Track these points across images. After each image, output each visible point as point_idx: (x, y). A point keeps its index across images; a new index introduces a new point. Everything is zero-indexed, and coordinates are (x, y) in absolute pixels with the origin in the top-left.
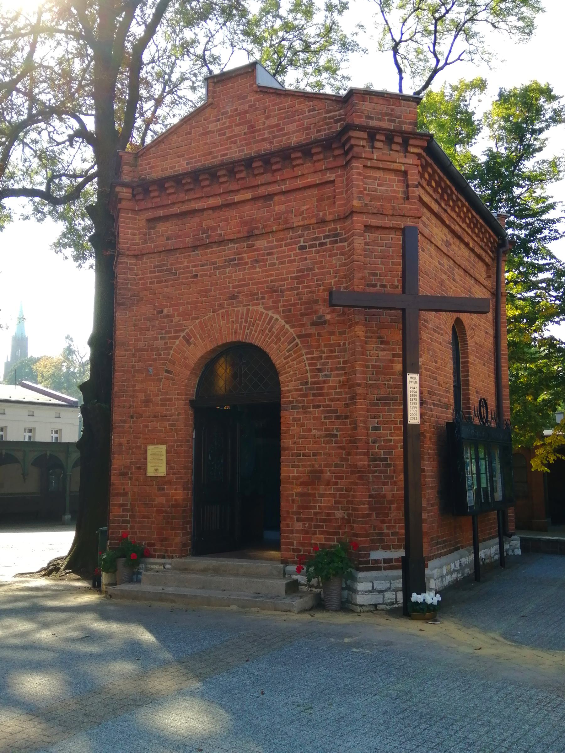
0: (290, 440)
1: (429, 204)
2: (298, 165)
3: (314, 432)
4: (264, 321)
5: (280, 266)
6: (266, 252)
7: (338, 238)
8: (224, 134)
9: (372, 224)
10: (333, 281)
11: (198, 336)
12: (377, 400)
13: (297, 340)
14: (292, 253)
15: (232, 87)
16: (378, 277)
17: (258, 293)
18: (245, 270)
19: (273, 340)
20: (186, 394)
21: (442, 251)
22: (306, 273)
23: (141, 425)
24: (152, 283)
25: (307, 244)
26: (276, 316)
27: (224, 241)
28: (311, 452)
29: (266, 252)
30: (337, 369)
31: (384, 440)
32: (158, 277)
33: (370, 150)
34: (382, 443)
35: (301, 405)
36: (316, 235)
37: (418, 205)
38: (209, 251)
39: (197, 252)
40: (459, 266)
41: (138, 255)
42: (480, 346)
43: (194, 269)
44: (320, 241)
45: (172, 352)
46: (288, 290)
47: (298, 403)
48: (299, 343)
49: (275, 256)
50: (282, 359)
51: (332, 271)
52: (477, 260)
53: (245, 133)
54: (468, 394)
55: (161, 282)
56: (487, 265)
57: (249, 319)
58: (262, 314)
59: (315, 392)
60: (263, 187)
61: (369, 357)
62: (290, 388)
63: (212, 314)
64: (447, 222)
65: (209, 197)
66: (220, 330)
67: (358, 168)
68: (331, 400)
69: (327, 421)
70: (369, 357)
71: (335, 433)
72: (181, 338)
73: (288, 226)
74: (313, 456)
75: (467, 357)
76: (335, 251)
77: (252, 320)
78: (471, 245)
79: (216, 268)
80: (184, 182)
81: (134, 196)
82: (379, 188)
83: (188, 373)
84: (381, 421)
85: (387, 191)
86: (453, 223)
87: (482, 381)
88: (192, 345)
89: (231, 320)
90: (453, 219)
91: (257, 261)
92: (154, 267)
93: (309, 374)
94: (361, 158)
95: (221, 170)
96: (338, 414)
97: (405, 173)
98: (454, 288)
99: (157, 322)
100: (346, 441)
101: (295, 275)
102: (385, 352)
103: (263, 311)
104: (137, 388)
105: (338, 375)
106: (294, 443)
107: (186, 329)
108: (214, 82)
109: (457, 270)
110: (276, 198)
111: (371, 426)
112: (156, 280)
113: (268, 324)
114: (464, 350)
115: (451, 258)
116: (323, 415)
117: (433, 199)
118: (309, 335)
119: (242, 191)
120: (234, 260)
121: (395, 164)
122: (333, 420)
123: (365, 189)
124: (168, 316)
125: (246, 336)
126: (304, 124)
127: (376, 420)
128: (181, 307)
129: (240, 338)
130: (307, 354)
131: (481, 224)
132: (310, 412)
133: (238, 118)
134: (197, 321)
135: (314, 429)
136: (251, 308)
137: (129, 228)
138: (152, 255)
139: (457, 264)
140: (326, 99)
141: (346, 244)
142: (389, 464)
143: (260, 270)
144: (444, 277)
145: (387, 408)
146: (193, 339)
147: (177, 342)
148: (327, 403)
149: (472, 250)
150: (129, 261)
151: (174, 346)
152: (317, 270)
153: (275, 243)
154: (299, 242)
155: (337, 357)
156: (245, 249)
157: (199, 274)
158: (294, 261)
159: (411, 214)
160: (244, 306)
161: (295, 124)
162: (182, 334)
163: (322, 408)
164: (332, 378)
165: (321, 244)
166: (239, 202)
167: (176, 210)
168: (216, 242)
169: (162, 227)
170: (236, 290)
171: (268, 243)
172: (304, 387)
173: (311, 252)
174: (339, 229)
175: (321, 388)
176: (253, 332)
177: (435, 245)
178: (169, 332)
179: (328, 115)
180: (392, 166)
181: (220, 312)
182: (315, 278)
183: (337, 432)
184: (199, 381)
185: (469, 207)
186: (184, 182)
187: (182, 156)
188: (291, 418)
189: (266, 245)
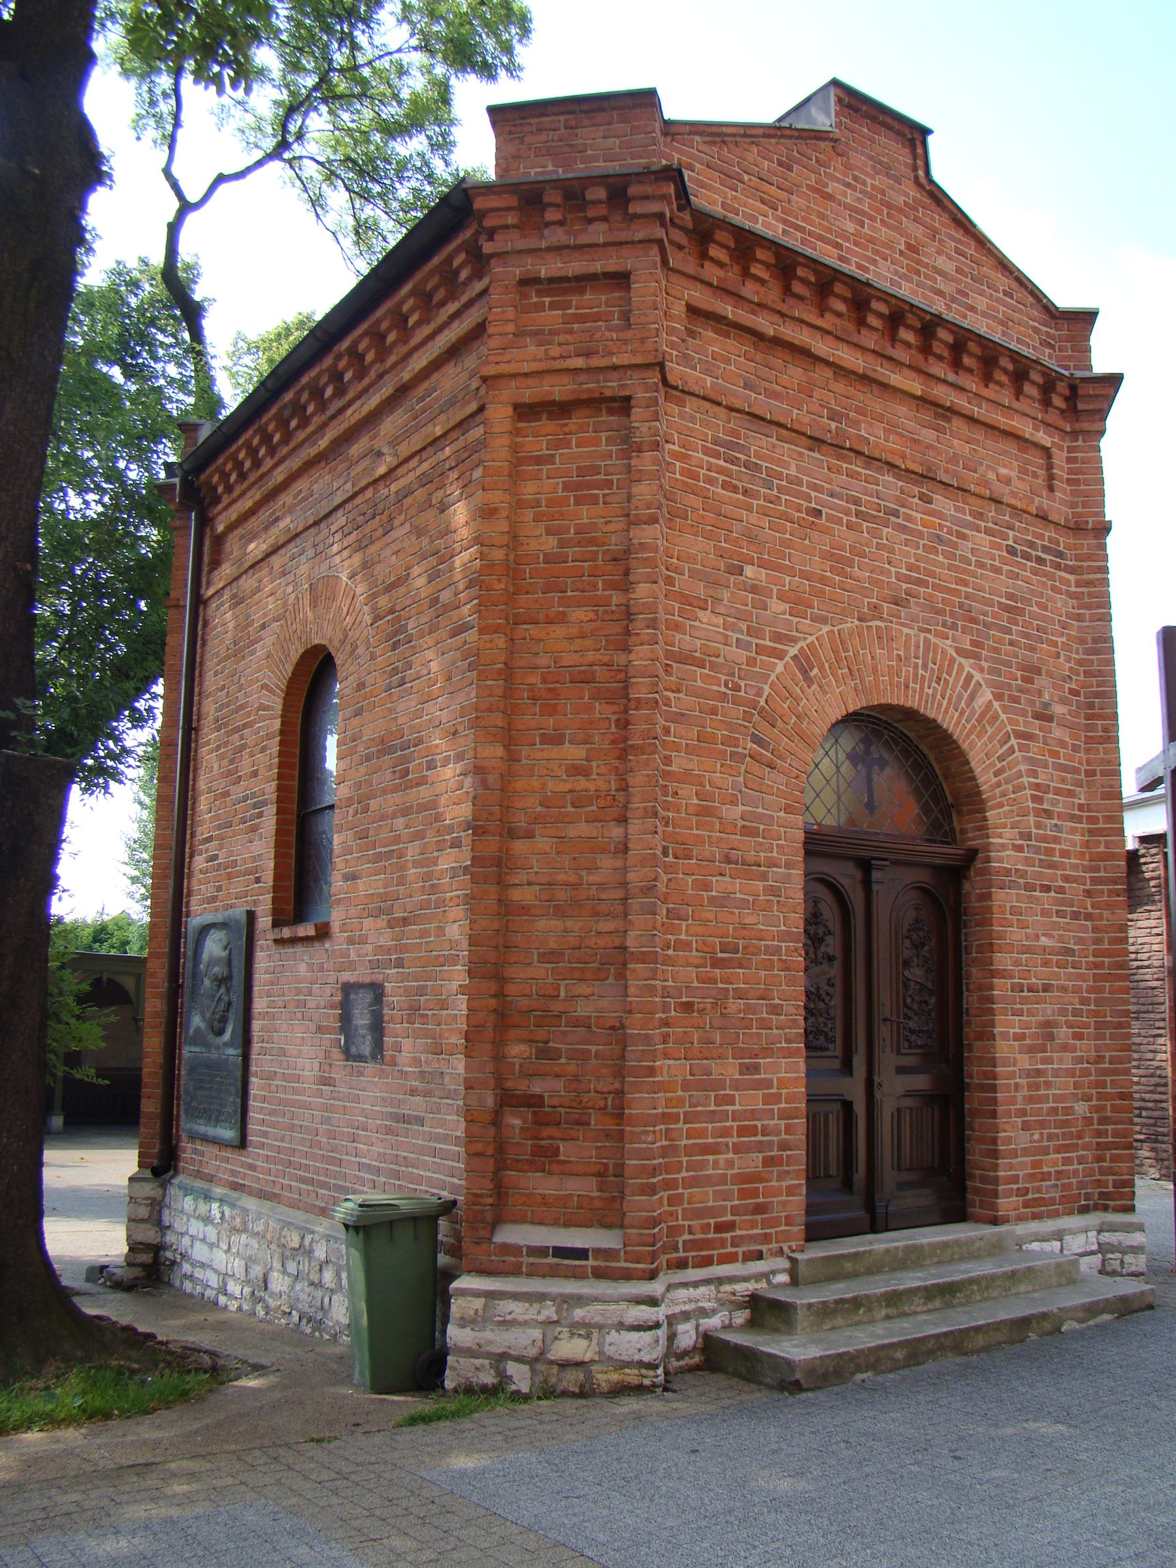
3: (1044, 940)
13: (1013, 741)
23: (690, 879)
24: (710, 481)
35: (1021, 881)
39: (816, 455)
45: (767, 690)
51: (775, 591)
68: (1066, 879)
88: (815, 687)
104: (674, 768)
119: (905, 370)
125: (927, 702)
129: (912, 702)
132: (1037, 898)
134: (826, 629)
135: (1044, 935)
138: (708, 405)
147: (780, 667)
151: (773, 677)
160: (921, 630)
163: (1053, 894)
166: (895, 390)
181: (873, 623)
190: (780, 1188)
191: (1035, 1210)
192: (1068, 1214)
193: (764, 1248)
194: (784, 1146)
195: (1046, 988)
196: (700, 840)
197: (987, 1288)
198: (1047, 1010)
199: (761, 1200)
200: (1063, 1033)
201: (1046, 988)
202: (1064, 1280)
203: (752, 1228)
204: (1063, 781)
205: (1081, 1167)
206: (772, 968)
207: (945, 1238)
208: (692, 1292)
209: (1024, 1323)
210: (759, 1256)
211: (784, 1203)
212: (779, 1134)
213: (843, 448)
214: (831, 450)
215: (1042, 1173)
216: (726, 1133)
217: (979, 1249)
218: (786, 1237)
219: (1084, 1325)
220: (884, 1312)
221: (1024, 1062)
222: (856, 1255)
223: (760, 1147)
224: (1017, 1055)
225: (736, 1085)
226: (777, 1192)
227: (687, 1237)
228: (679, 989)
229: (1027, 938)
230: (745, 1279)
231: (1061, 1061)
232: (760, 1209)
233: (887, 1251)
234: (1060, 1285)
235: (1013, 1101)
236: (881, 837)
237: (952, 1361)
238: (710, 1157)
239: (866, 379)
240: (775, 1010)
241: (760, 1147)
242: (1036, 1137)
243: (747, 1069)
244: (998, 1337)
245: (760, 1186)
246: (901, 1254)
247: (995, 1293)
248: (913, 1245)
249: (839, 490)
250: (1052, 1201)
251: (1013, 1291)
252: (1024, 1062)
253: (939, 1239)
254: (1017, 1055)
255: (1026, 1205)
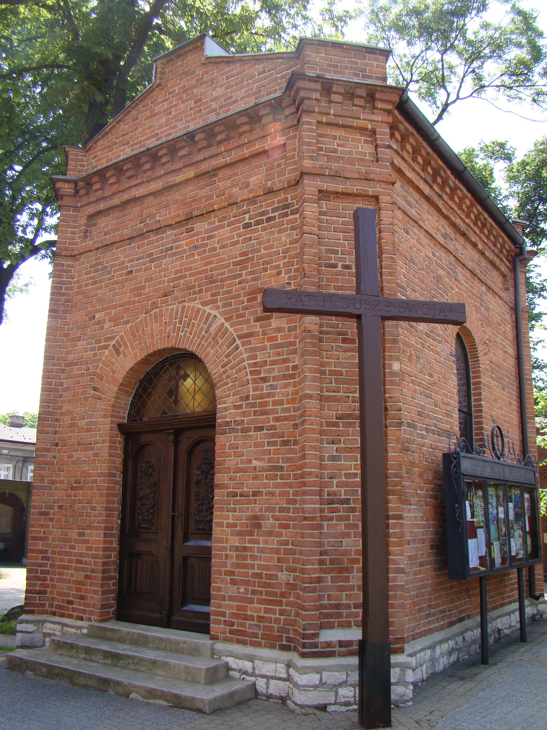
0: (226, 475)
1: (416, 182)
2: (245, 132)
3: (255, 463)
4: (200, 321)
5: (221, 251)
6: (206, 235)
7: (289, 210)
8: (170, 113)
9: (329, 189)
10: (281, 263)
11: (128, 343)
12: (337, 419)
13: (238, 342)
14: (235, 233)
15: (182, 66)
16: (340, 255)
17: (195, 285)
18: (182, 259)
19: (210, 343)
20: (112, 416)
21: (436, 240)
22: (250, 256)
23: (66, 454)
24: (86, 285)
25: (252, 221)
26: (214, 312)
27: (161, 228)
28: (250, 490)
29: (206, 235)
30: (285, 377)
31: (345, 474)
32: (93, 278)
33: (328, 105)
34: (344, 479)
35: (239, 427)
36: (263, 209)
37: (390, 170)
38: (145, 241)
40: (464, 265)
41: (75, 256)
42: (497, 366)
43: (129, 264)
44: (268, 216)
45: (100, 365)
46: (229, 278)
47: (237, 425)
48: (240, 345)
49: (216, 239)
50: (220, 367)
52: (490, 267)
53: (191, 109)
54: (481, 423)
55: (95, 283)
56: (504, 276)
57: (184, 319)
58: (199, 310)
59: (258, 409)
60: (207, 162)
61: (325, 360)
62: (228, 405)
63: (144, 315)
64: (444, 211)
65: (149, 181)
66: (152, 335)
67: (309, 123)
68: (277, 419)
69: (272, 448)
70: (325, 360)
71: (280, 464)
72: (111, 347)
73: (231, 201)
74: (253, 496)
75: (479, 377)
76: (285, 226)
77: (187, 319)
78: (480, 246)
79: (151, 261)
80: (125, 168)
81: (77, 192)
82: (340, 148)
83: (116, 389)
84: (341, 448)
85: (350, 152)
86: (452, 214)
87: (501, 409)
88: (122, 355)
89: (164, 321)
90: (452, 208)
91: (196, 247)
92: (91, 267)
93: (251, 386)
94: (314, 112)
95: (161, 149)
96: (285, 438)
97: (373, 132)
98: (457, 290)
99: (89, 330)
100: (294, 475)
101: (239, 259)
102: (349, 354)
103: (200, 307)
104: (64, 410)
105: (286, 386)
106: (230, 479)
107: (116, 336)
108: (162, 64)
109: (459, 269)
110: (221, 174)
111: (327, 455)
112: (91, 281)
113: (205, 323)
114: (475, 368)
115: (450, 252)
116: (266, 440)
117: (422, 178)
118: (251, 335)
120: (171, 248)
121: (358, 121)
122: (278, 447)
123: (320, 149)
124: (99, 323)
126: (253, 89)
127: (335, 446)
128: (113, 311)
129: (171, 343)
130: (249, 358)
131: (490, 224)
132: (251, 436)
133: (185, 95)
134: (129, 326)
135: (255, 459)
136: (186, 304)
137: (70, 227)
138: (88, 254)
139: (459, 261)
140: (278, 58)
141: (297, 216)
142: (353, 508)
143: (199, 257)
144: (441, 272)
145: (351, 429)
146: (123, 347)
147: (107, 352)
148: (272, 423)
149: (483, 254)
150: (65, 263)
152: (263, 251)
153: (217, 224)
154: (244, 219)
155: (285, 361)
156: (184, 234)
157: (134, 269)
158: (237, 242)
159: (381, 179)
161: (243, 90)
162: (112, 343)
163: (265, 431)
164: (279, 390)
165: (269, 219)
166: (180, 183)
167: (116, 201)
168: (152, 231)
169: (103, 222)
170: (171, 284)
171: (209, 224)
172: (244, 403)
173: (256, 230)
174: (289, 199)
175: (266, 404)
176: (188, 334)
177: (425, 231)
178: (97, 342)
179: (279, 75)
180: (355, 123)
181: (152, 312)
182: (261, 261)
183: (283, 462)
184: (132, 401)
185: (473, 200)
186: (125, 168)
187: (128, 143)
188: (228, 444)
189: (207, 227)
190: (91, 590)
191: (240, 637)
192: (270, 647)
193: (84, 616)
194: (93, 571)
195: (255, 494)
196: (70, 437)
197: (138, 664)
198: (256, 508)
199: (83, 593)
200: (269, 523)
201: (255, 494)
202: (190, 678)
203: (79, 605)
204: (278, 354)
205: (282, 618)
206: (93, 489)
207: (161, 635)
208: (52, 626)
209: (106, 682)
210: (82, 619)
211: (92, 597)
212: (91, 565)
213: (144, 234)
214: (139, 238)
215: (246, 615)
216: (71, 561)
217: (183, 649)
218: (92, 613)
219: (146, 700)
220: (83, 656)
221: (235, 541)
222: (113, 630)
223: (83, 569)
224: (229, 537)
225: (76, 541)
226: (89, 591)
227: (57, 603)
228: (58, 500)
229: (242, 463)
230: (73, 627)
231: (266, 542)
232: (82, 597)
233: (128, 633)
234: (186, 680)
235: (225, 565)
236: (170, 418)
237: (65, 684)
238: (66, 571)
239: (168, 188)
240: (93, 509)
241: (83, 569)
242: (242, 590)
243: (82, 534)
244: (91, 683)
245: (83, 587)
246: (135, 637)
247: (142, 669)
248: (142, 634)
249: (142, 255)
250: (256, 635)
251: (154, 672)
252: (235, 541)
253: (158, 635)
254: (229, 537)
255: (232, 632)
